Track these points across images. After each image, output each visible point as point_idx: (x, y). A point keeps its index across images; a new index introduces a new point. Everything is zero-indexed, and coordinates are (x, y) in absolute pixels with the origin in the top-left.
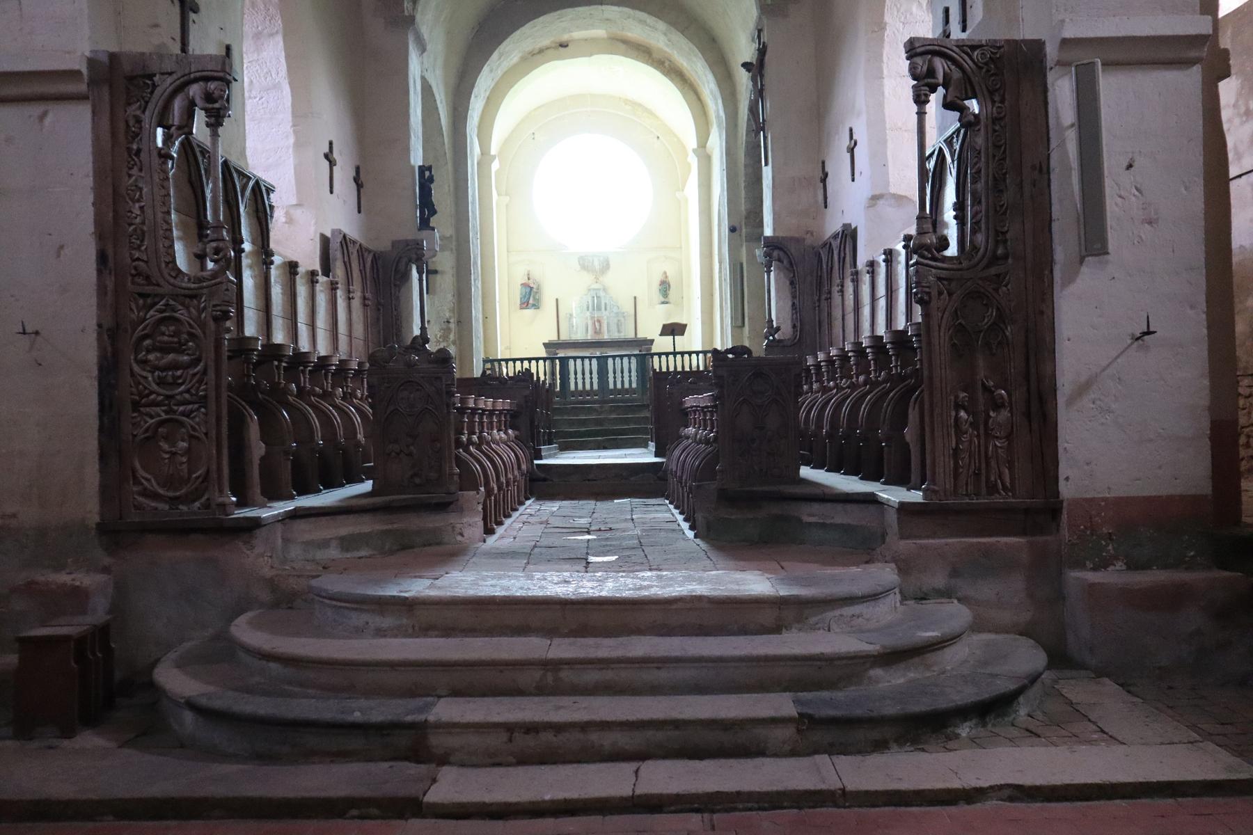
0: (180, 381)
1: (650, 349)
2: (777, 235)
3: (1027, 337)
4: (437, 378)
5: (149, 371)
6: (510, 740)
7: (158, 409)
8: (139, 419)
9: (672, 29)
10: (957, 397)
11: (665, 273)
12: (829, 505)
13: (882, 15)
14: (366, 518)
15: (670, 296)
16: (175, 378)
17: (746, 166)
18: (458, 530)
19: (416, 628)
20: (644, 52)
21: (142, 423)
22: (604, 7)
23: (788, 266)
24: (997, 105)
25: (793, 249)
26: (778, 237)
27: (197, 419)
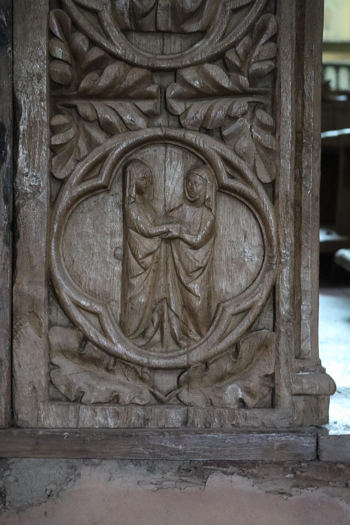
0: (193, 27)
8: (71, 133)
21: (82, 144)
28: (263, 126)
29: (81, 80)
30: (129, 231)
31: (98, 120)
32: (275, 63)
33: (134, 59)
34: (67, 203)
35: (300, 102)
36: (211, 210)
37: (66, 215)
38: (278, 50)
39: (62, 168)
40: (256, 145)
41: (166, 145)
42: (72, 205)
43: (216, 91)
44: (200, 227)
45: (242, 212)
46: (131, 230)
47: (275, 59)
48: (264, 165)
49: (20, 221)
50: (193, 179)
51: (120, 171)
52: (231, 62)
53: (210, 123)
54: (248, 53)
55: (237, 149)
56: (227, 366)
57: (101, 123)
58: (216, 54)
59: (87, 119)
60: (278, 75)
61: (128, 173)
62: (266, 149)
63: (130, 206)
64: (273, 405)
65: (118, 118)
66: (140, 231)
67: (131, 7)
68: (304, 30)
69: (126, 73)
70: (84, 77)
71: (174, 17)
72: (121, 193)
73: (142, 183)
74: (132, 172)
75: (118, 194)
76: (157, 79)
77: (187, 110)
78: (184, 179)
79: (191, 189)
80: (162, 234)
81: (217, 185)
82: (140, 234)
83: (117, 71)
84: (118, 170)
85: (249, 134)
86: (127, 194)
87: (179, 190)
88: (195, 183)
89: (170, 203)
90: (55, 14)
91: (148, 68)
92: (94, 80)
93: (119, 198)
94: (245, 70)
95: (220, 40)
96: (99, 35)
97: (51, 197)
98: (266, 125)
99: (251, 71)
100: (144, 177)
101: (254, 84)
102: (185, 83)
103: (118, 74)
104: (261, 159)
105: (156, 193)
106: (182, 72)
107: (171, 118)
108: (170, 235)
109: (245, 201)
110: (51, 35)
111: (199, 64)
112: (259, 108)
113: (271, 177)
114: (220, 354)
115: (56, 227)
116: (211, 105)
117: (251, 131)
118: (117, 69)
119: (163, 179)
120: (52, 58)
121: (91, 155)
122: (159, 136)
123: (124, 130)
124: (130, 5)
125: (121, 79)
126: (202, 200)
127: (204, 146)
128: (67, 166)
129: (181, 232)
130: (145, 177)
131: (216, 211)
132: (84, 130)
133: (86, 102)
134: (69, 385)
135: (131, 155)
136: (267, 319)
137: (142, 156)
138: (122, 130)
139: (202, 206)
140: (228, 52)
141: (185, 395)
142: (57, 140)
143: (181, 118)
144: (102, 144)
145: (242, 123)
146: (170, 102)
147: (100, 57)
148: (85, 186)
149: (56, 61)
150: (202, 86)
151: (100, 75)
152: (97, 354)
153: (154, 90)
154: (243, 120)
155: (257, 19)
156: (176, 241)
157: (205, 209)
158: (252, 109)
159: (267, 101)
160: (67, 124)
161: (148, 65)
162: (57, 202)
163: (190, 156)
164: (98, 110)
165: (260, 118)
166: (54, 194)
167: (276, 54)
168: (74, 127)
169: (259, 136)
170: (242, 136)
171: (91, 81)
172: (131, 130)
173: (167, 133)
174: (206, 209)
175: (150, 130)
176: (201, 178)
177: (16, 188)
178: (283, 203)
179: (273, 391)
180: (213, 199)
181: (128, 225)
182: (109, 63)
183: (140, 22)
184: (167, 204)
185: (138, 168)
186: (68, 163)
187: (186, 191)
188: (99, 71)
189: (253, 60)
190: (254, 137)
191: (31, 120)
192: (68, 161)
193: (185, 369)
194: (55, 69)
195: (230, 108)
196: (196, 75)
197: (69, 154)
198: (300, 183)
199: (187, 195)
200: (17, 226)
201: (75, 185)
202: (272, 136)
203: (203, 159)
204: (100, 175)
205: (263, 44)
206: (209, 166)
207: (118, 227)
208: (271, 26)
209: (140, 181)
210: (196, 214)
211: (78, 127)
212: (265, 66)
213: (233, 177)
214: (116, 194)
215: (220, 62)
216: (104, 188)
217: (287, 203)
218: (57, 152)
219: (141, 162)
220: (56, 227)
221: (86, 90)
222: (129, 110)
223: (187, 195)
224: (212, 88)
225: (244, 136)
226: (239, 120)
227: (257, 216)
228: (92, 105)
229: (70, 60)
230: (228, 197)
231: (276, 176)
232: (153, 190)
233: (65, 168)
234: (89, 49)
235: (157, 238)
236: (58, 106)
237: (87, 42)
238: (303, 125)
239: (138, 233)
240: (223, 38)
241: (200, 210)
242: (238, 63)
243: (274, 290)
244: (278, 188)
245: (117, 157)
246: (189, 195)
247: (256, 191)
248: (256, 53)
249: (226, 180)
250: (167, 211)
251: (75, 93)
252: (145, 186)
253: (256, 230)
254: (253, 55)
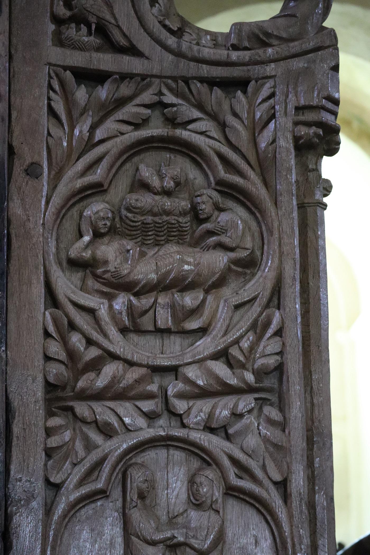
0: (193, 325)
8: (67, 435)
21: (79, 446)
28: (271, 422)
29: (77, 380)
30: (131, 538)
31: (96, 422)
32: (282, 358)
33: (133, 357)
34: (64, 509)
35: (309, 398)
36: (218, 512)
37: (63, 523)
38: (284, 344)
39: (58, 472)
40: (264, 443)
41: (167, 447)
42: (69, 511)
43: (220, 388)
44: (207, 532)
45: (252, 516)
46: (133, 537)
48: (274, 463)
49: (12, 530)
50: (198, 480)
51: (120, 476)
52: (234, 357)
53: (215, 421)
54: (252, 348)
55: (245, 446)
57: (100, 424)
58: (220, 349)
59: (84, 421)
60: (285, 369)
61: (129, 476)
62: (275, 446)
63: (132, 511)
65: (117, 419)
66: (143, 537)
67: (129, 306)
68: (309, 325)
69: (125, 372)
70: (81, 378)
71: (174, 316)
72: (121, 500)
73: (144, 486)
74: (133, 475)
75: (118, 500)
76: (157, 379)
77: (189, 409)
78: (188, 483)
79: (197, 491)
80: (166, 541)
81: (224, 487)
82: (142, 541)
83: (116, 370)
84: (118, 474)
85: (256, 432)
86: (128, 498)
87: (184, 496)
88: (201, 484)
89: (173, 510)
90: (50, 314)
91: (148, 366)
92: (91, 379)
93: (119, 504)
94: (249, 366)
95: (223, 336)
96: (96, 334)
97: (46, 505)
98: (275, 420)
99: (256, 366)
100: (146, 480)
101: (260, 381)
102: (188, 381)
103: (117, 373)
104: (271, 457)
105: (158, 499)
106: (184, 370)
107: (173, 418)
108: (175, 541)
109: (255, 503)
110: (47, 334)
111: (201, 361)
112: (267, 405)
113: (282, 475)
115: (52, 533)
116: (215, 403)
117: (258, 429)
118: (115, 368)
119: (165, 483)
121: (89, 458)
122: (162, 436)
123: (124, 431)
124: (128, 304)
125: (120, 378)
126: (209, 501)
127: (209, 445)
128: (63, 470)
129: (186, 537)
130: (147, 479)
131: (223, 514)
132: (81, 431)
133: (83, 403)
135: (131, 458)
137: (142, 460)
138: (121, 431)
139: (208, 509)
140: (232, 348)
142: (53, 442)
143: (184, 417)
144: (101, 446)
145: (249, 420)
146: (172, 401)
147: (97, 356)
148: (84, 490)
149: (52, 362)
150: (205, 383)
151: (98, 375)
153: (155, 388)
154: (250, 417)
155: (261, 313)
156: (182, 548)
157: (212, 512)
158: (258, 407)
159: (274, 398)
160: (64, 425)
161: (148, 363)
162: (53, 509)
163: (194, 459)
164: (96, 410)
165: (268, 414)
166: (49, 501)
167: (282, 348)
168: (70, 430)
169: (268, 433)
170: (250, 434)
171: (89, 380)
172: (131, 431)
173: (170, 433)
174: (213, 512)
175: (151, 430)
176: (207, 478)
177: (8, 494)
178: (296, 502)
180: (220, 500)
181: (130, 532)
182: (107, 363)
183: (138, 320)
184: (171, 511)
185: (139, 470)
186: (65, 467)
187: (191, 494)
188: (97, 372)
189: (258, 355)
190: (262, 435)
191: (25, 422)
192: (64, 465)
194: (51, 370)
195: (236, 405)
196: (198, 373)
197: (66, 458)
198: (313, 483)
199: (192, 498)
200: (9, 535)
201: (72, 490)
202: (281, 432)
203: (208, 459)
204: (99, 478)
205: (268, 339)
206: (214, 466)
207: (118, 530)
209: (142, 484)
210: (202, 518)
211: (74, 430)
212: (272, 361)
213: (241, 478)
214: (115, 500)
215: (223, 359)
217: (301, 502)
218: (53, 456)
219: (142, 465)
220: (52, 533)
221: (83, 390)
222: (128, 410)
223: (192, 498)
224: (215, 386)
225: (251, 434)
226: (245, 418)
227: (269, 518)
228: (89, 406)
229: (66, 359)
230: (235, 500)
231: (288, 474)
232: (155, 495)
233: (61, 472)
234: (86, 349)
235: (161, 546)
236: (53, 409)
237: (84, 341)
238: (313, 422)
239: (141, 540)
240: (225, 334)
241: (207, 514)
242: (242, 358)
244: (290, 486)
245: (117, 458)
246: (194, 498)
247: (267, 490)
248: (261, 347)
250: (170, 517)
251: (72, 394)
252: (147, 489)
253: (267, 533)
254: (257, 350)
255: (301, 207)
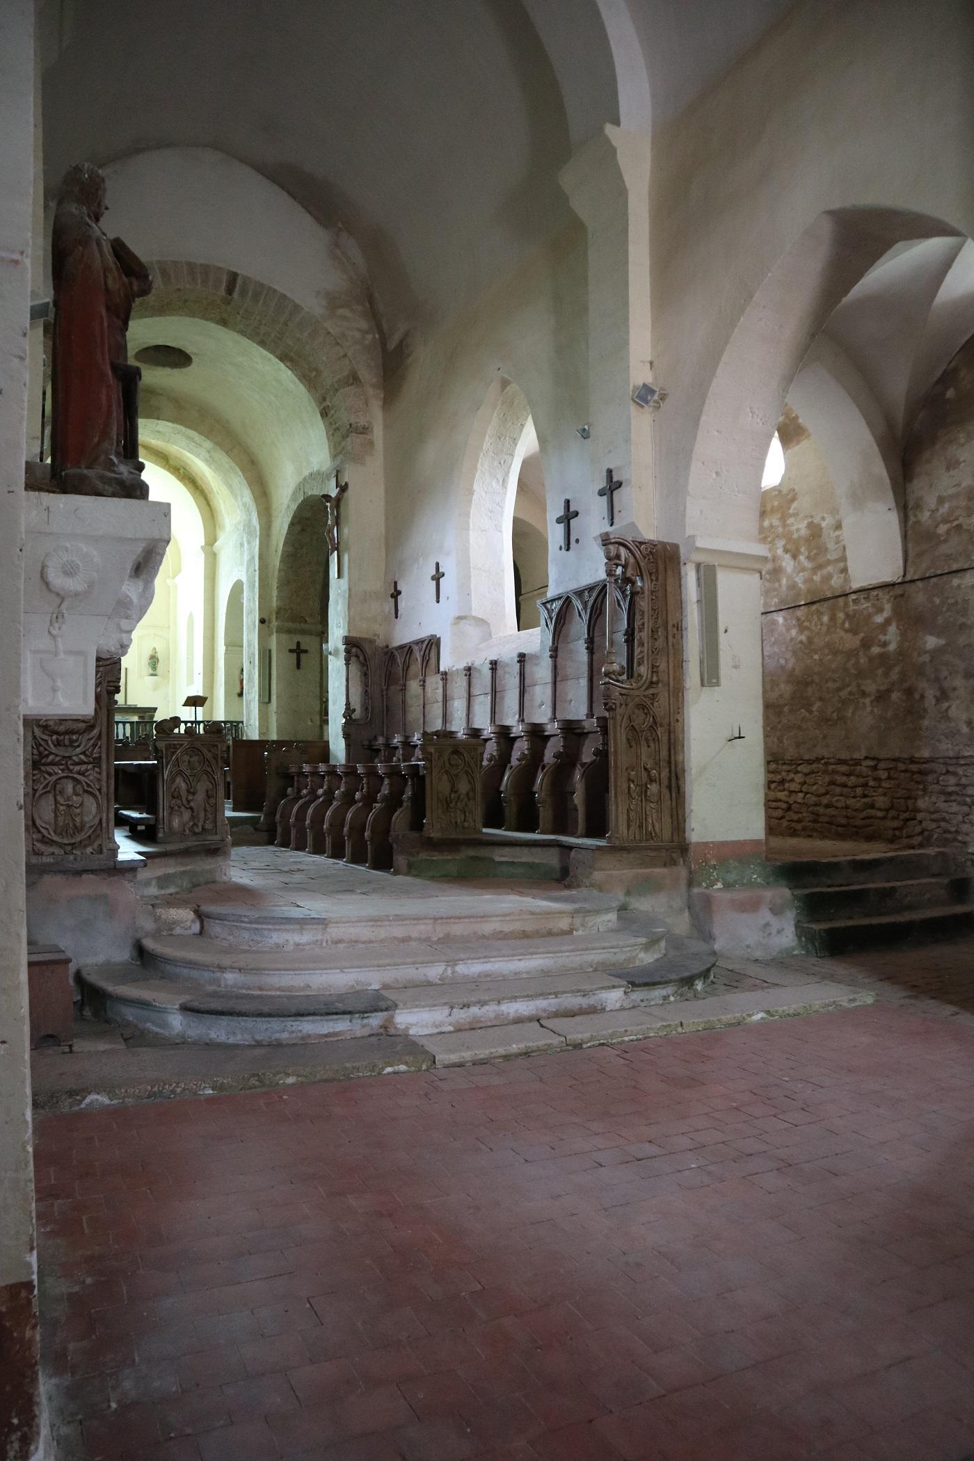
0: (77, 744)
1: (153, 716)
2: (351, 635)
3: (669, 736)
4: (214, 746)
5: (49, 735)
6: (450, 1015)
7: (56, 769)
9: (218, 448)
10: (629, 774)
11: (155, 649)
12: (518, 849)
13: (472, 485)
14: (172, 861)
15: (158, 669)
16: (72, 741)
17: (280, 570)
18: (223, 871)
19: (329, 942)
20: (162, 458)
21: (42, 779)
22: (160, 422)
23: (363, 661)
24: (654, 582)
25: (367, 647)
26: (352, 637)
27: (91, 778)
28: (97, 773)
47: (100, 753)
56: (87, 842)
64: (101, 853)
110: (33, 747)
114: (84, 840)
120: (33, 754)
130: (920, 816)
134: (39, 850)
136: (99, 828)
141: (74, 852)
142: (34, 778)
152: (47, 840)
179: (101, 849)
193: (74, 844)
207: (53, 802)
208: (99, 743)
216: (49, 792)
243: (101, 820)
249: (86, 788)
255: (108, 710)
